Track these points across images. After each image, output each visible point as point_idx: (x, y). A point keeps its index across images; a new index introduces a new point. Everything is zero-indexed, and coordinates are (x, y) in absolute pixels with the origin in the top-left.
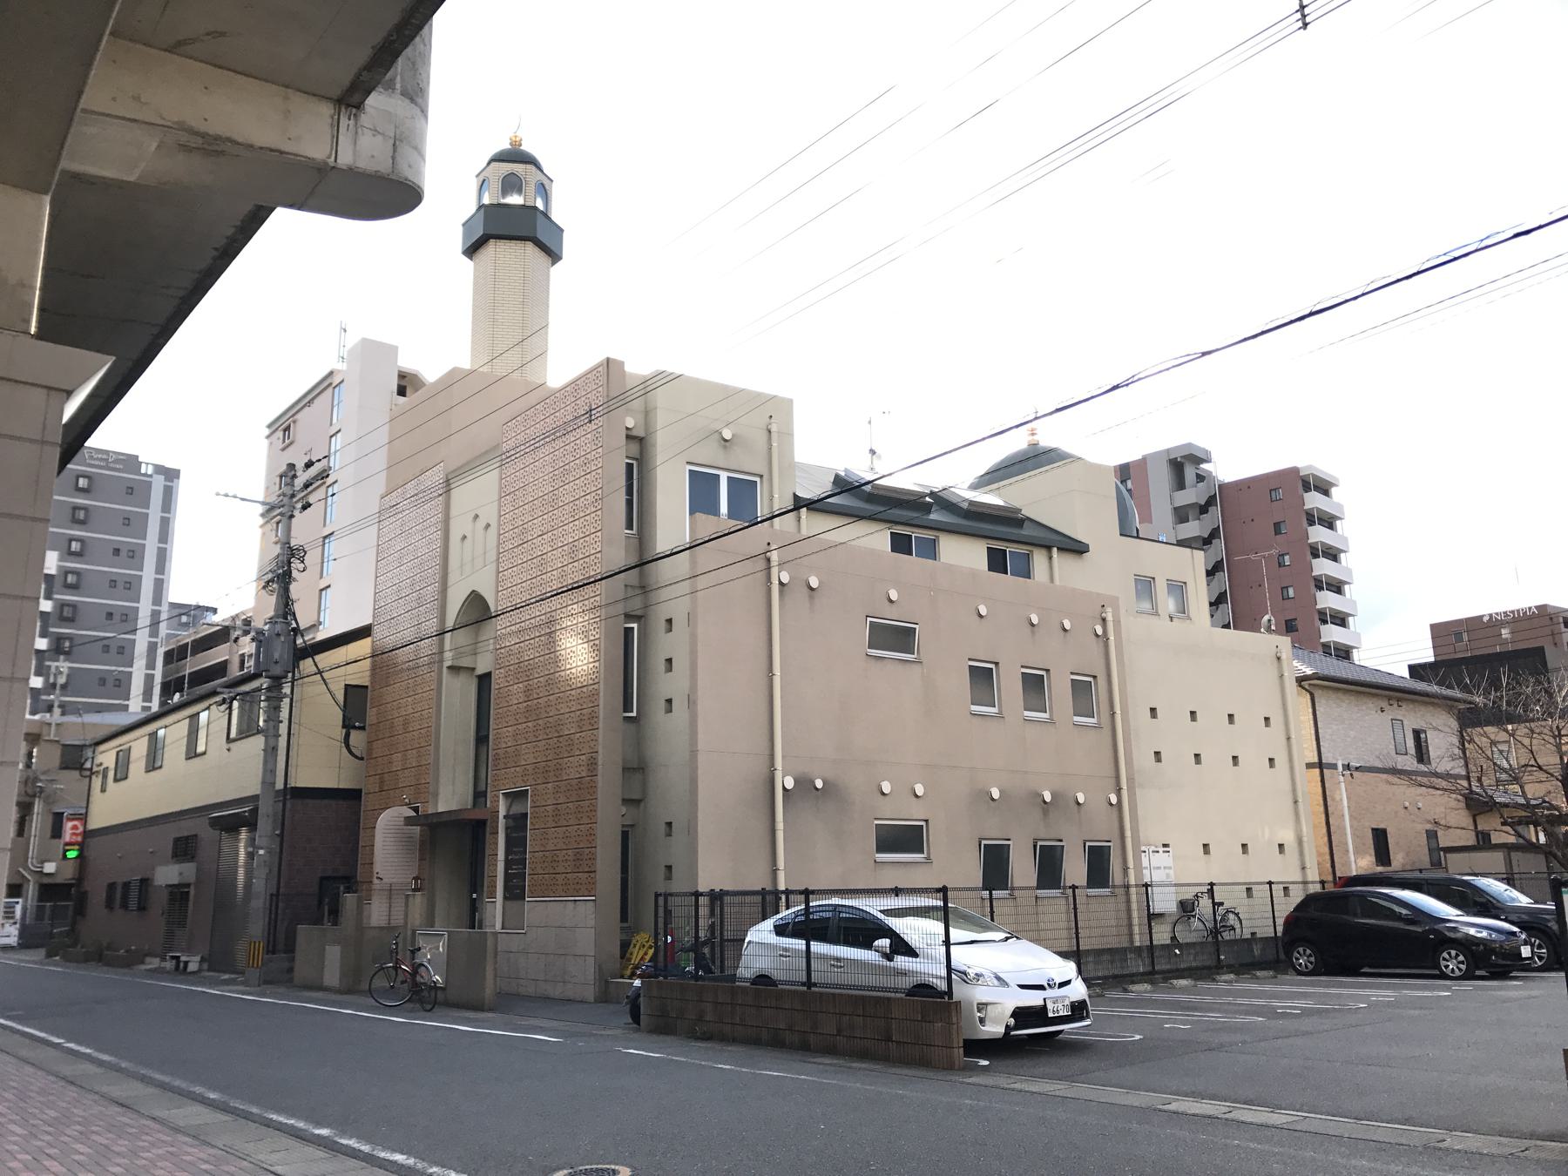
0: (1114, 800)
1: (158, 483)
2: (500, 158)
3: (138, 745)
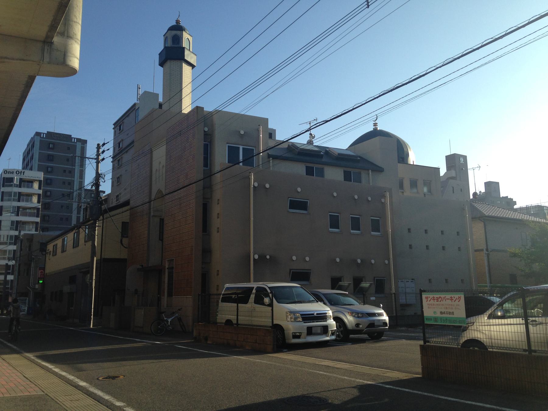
0: (387, 262)
1: (79, 145)
2: (172, 28)
3: (59, 242)
